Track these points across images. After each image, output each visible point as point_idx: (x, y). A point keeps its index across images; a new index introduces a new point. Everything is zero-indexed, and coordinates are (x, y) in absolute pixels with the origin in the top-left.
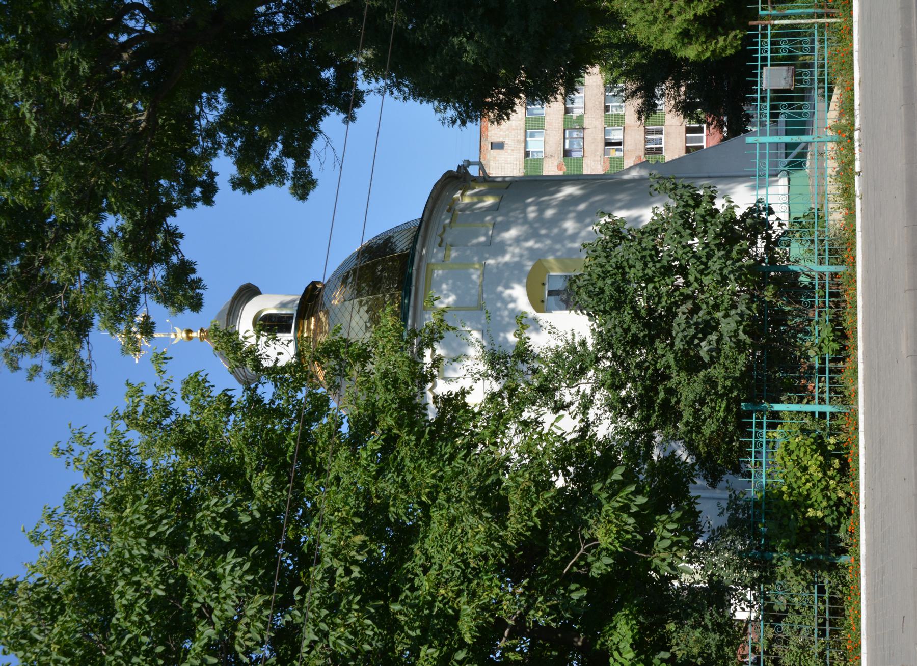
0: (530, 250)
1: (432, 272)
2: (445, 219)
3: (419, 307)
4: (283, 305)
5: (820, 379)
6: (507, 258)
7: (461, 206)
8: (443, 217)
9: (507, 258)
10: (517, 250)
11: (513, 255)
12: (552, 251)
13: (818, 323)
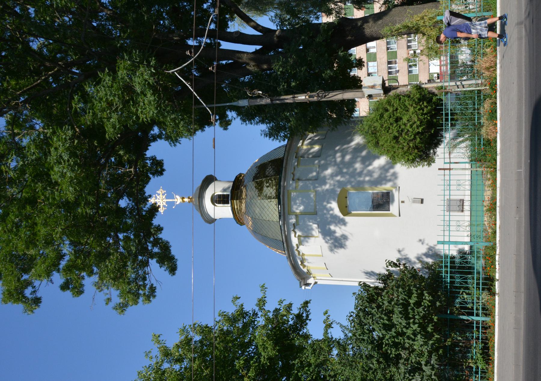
0: (339, 181)
1: (291, 194)
2: (295, 162)
3: (286, 214)
4: (224, 190)
5: (476, 376)
6: (327, 187)
7: (303, 151)
8: (294, 161)
9: (327, 187)
10: (332, 182)
11: (330, 185)
12: (350, 182)
13: (475, 348)
